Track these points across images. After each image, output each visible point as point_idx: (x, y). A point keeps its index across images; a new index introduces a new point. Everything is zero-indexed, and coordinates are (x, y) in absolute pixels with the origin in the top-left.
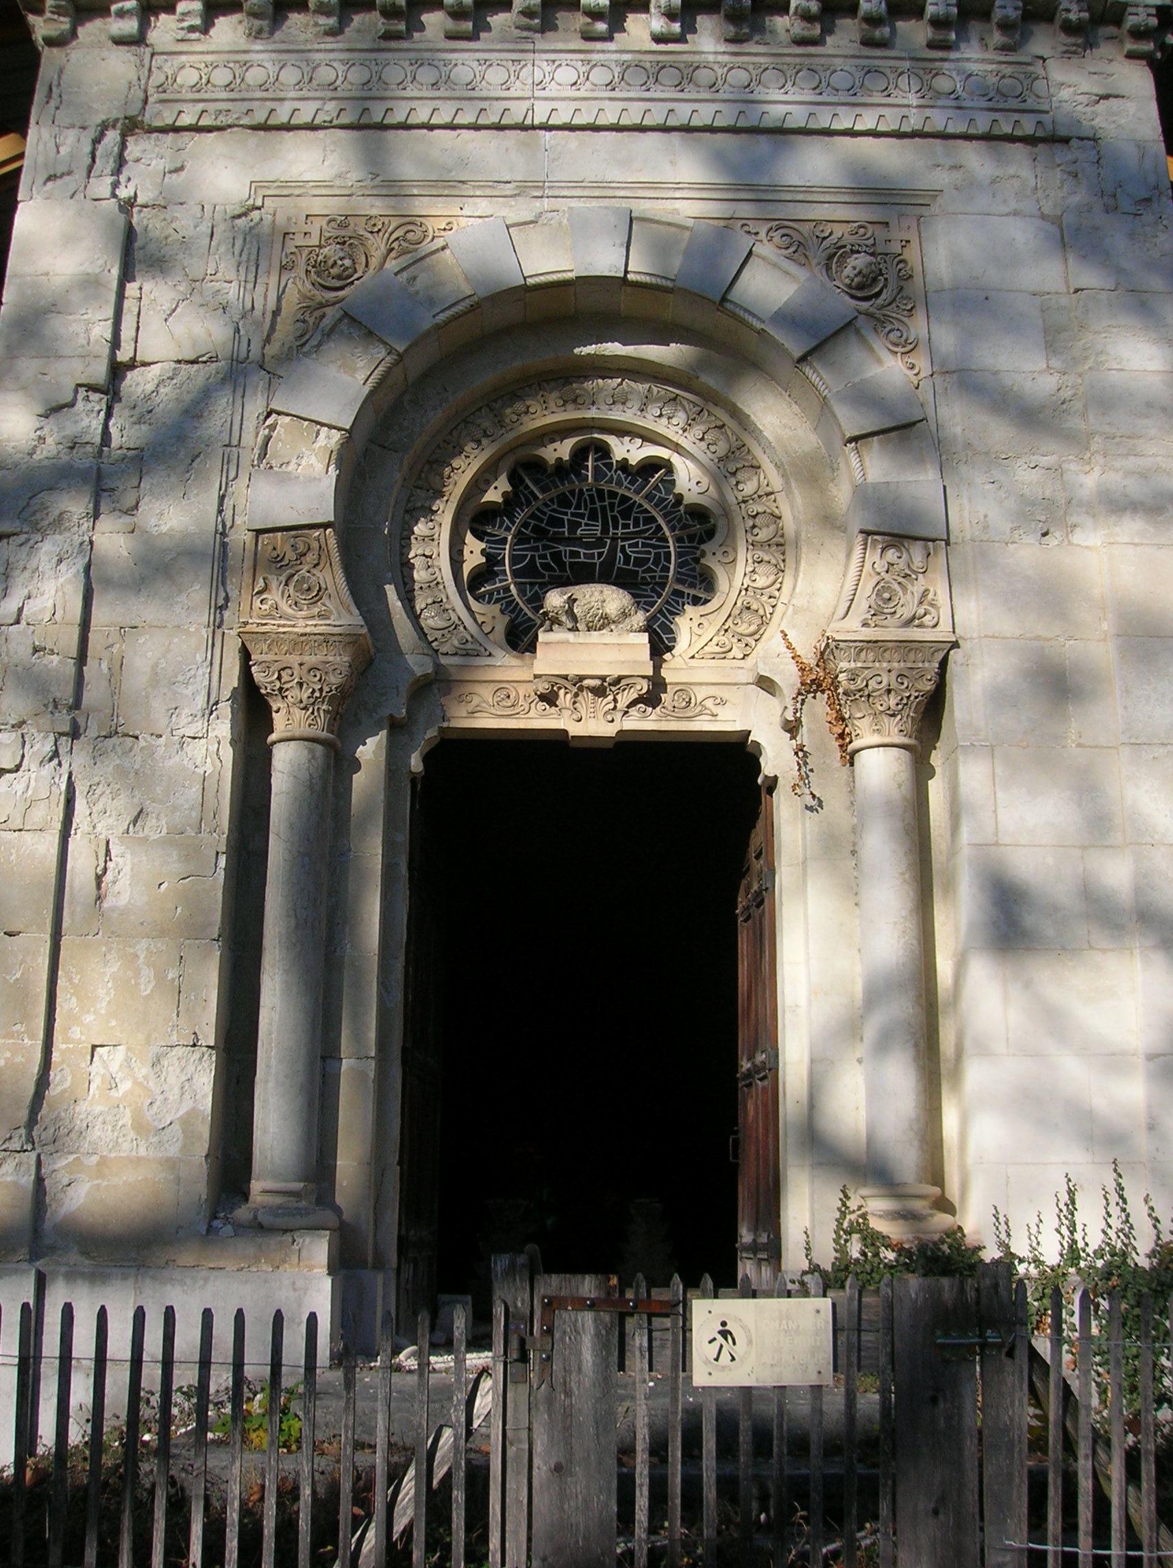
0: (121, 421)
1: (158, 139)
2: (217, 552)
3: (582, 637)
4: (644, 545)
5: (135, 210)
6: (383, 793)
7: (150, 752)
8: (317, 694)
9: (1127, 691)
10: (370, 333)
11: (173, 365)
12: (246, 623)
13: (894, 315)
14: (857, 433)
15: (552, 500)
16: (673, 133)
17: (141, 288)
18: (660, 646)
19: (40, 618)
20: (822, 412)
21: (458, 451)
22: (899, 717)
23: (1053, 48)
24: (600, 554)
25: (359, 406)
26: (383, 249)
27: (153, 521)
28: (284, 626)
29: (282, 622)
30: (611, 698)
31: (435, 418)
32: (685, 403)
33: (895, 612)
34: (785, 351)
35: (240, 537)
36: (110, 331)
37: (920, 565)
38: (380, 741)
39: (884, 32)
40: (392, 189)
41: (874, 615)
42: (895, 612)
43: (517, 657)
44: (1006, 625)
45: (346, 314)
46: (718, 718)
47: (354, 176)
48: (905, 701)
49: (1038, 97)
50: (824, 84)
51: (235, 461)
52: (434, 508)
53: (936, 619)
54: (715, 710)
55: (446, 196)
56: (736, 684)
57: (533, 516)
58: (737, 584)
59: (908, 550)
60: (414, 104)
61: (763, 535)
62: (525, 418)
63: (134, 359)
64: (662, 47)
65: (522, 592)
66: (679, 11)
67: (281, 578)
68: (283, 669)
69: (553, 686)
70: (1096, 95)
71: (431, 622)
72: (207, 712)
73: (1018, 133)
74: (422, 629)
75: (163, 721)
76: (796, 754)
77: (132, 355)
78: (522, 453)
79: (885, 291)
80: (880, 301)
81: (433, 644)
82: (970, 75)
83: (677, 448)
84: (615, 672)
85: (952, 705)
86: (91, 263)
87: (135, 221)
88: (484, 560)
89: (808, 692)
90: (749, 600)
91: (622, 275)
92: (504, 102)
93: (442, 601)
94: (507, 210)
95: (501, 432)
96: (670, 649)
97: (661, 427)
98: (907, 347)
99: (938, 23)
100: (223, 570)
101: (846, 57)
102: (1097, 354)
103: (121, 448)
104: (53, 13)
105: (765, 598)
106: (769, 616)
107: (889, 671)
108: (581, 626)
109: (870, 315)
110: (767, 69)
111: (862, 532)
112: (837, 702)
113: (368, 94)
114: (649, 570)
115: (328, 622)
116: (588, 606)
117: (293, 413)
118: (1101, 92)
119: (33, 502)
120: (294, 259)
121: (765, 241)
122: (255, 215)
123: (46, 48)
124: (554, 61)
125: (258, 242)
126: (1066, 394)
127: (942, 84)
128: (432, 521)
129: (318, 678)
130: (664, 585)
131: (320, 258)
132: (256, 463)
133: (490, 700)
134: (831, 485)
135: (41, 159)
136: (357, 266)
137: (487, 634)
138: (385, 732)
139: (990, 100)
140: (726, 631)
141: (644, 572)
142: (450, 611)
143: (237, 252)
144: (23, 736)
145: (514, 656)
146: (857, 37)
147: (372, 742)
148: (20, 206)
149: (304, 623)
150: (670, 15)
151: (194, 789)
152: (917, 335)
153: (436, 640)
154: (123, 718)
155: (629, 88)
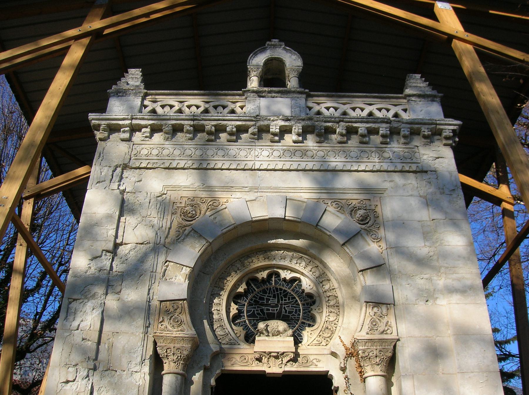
0: (117, 262)
1: (134, 171)
2: (147, 308)
3: (271, 338)
4: (292, 306)
5: (125, 193)
6: (201, 393)
7: (120, 376)
8: (179, 358)
9: (458, 354)
11: (135, 245)
12: (156, 333)
13: (373, 229)
14: (362, 269)
15: (260, 291)
16: (300, 172)
17: (126, 219)
18: (297, 341)
19: (85, 328)
20: (351, 262)
21: (229, 275)
22: (380, 365)
23: (420, 143)
24: (277, 310)
25: (196, 260)
26: (206, 208)
27: (126, 297)
28: (169, 334)
29: (168, 332)
30: (280, 359)
31: (221, 264)
32: (305, 259)
33: (377, 329)
34: (338, 242)
35: (155, 303)
36: (115, 233)
37: (385, 313)
38: (201, 374)
39: (367, 139)
40: (209, 189)
41: (370, 330)
42: (377, 329)
43: (248, 345)
44: (416, 333)
45: (193, 229)
46: (318, 366)
47: (197, 184)
48: (382, 360)
49: (416, 158)
50: (348, 156)
51: (154, 277)
52: (221, 294)
53: (391, 331)
54: (317, 363)
55: (227, 191)
56: (323, 354)
57: (254, 297)
58: (323, 320)
59: (381, 308)
60: (217, 162)
61: (332, 303)
62: (251, 264)
63: (122, 242)
64: (296, 145)
65: (250, 323)
66: (301, 133)
67: (168, 317)
68: (168, 349)
69: (261, 355)
70: (435, 157)
71: (219, 333)
72: (141, 363)
73: (411, 170)
74: (216, 335)
75: (126, 366)
76: (345, 379)
77: (121, 241)
78: (250, 276)
79: (370, 221)
80: (368, 225)
81: (220, 341)
82: (395, 152)
83: (302, 274)
84: (282, 350)
85: (398, 359)
86: (110, 210)
87: (125, 197)
88: (237, 312)
89: (349, 357)
90: (327, 325)
91: (284, 217)
92: (245, 162)
93: (223, 326)
94: (246, 196)
95: (244, 269)
96: (301, 342)
97: (297, 267)
98: (378, 240)
99: (383, 136)
100: (149, 314)
101: (355, 147)
102: (441, 240)
103: (116, 272)
104: (103, 131)
105: (333, 325)
106: (334, 331)
107: (376, 349)
108: (270, 334)
109: (366, 230)
110: (330, 151)
111: (365, 302)
112: (359, 360)
113: (202, 158)
114: (293, 315)
115: (184, 333)
116: (273, 328)
117: (174, 262)
118: (437, 156)
119: (86, 288)
120: (176, 211)
121: (330, 206)
122: (164, 196)
123: (100, 141)
124: (262, 149)
125: (165, 205)
126: (431, 254)
127: (386, 155)
128: (220, 298)
129: (180, 352)
130: (299, 320)
131: (185, 211)
132: (161, 278)
133: (239, 360)
134: (354, 286)
135: (95, 176)
136: (197, 213)
137: (238, 337)
138: (202, 371)
139: (401, 160)
140: (320, 336)
141: (291, 316)
142: (226, 329)
143: (158, 208)
144: (77, 369)
145: (247, 345)
146: (358, 141)
147: (198, 374)
148: (88, 191)
149: (176, 333)
150: (299, 135)
151: (135, 390)
152: (381, 236)
153: (221, 339)
154: (112, 364)
155: (285, 157)
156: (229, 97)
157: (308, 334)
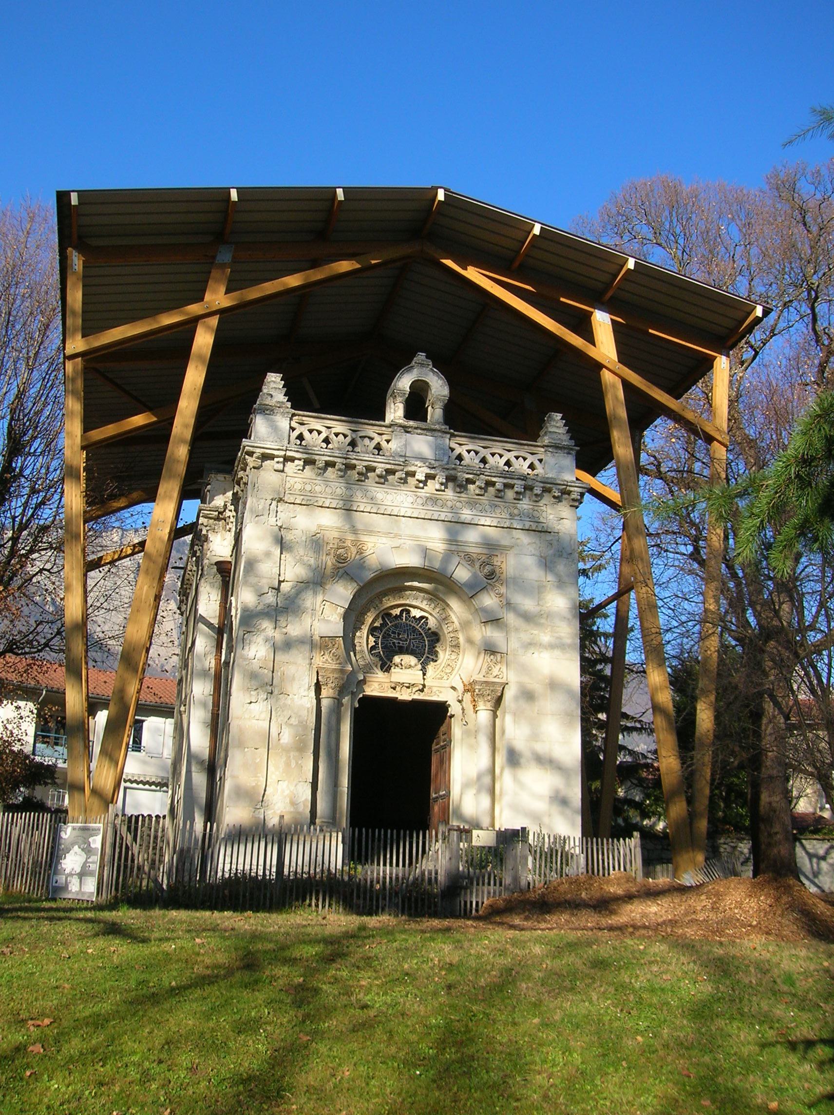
10: (352, 578)
40: (354, 530)
64: (438, 493)
78: (385, 612)
80: (494, 580)
83: (431, 614)
99: (517, 493)
156: (376, 428)
157: (430, 668)
